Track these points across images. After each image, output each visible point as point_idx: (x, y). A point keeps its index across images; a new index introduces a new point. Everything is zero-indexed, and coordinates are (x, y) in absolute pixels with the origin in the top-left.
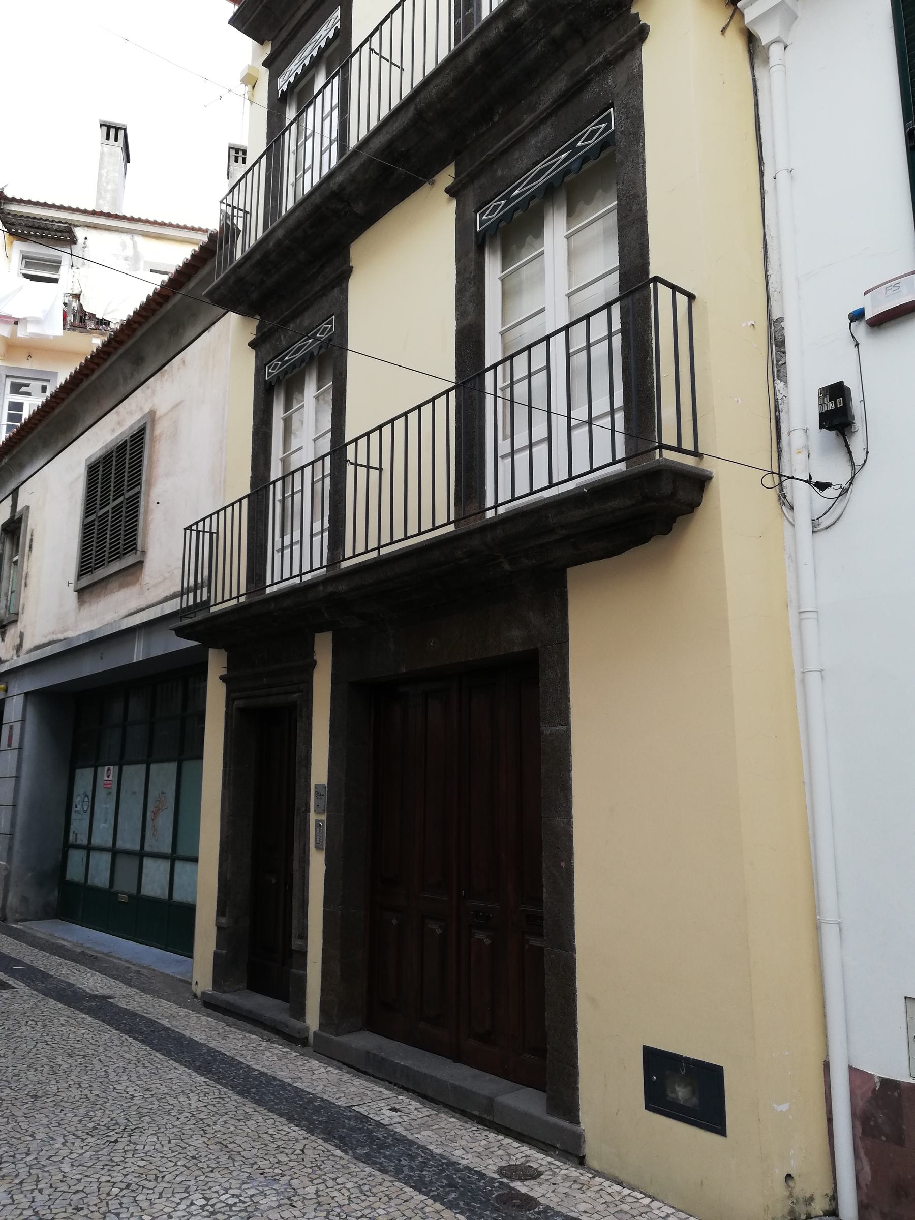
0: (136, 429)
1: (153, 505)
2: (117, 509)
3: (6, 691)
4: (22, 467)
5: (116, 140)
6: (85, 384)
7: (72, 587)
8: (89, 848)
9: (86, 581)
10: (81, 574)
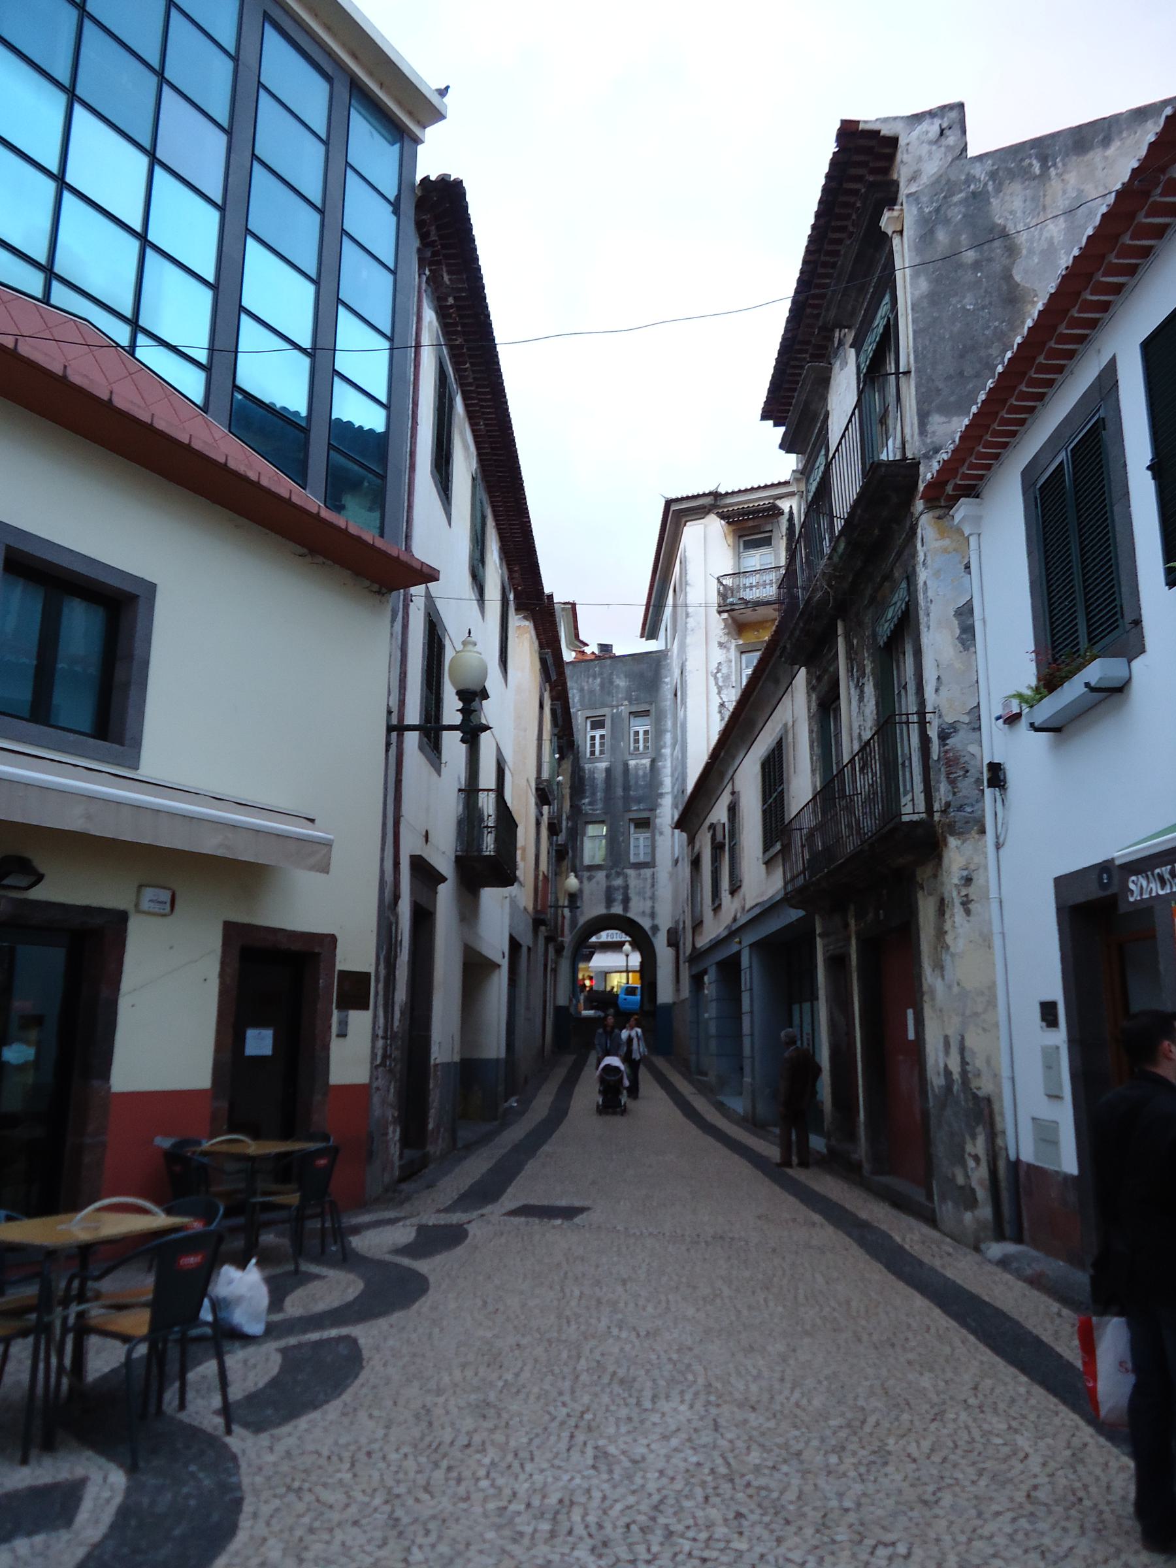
0: (779, 736)
3: (740, 942)
4: (734, 758)
7: (761, 861)
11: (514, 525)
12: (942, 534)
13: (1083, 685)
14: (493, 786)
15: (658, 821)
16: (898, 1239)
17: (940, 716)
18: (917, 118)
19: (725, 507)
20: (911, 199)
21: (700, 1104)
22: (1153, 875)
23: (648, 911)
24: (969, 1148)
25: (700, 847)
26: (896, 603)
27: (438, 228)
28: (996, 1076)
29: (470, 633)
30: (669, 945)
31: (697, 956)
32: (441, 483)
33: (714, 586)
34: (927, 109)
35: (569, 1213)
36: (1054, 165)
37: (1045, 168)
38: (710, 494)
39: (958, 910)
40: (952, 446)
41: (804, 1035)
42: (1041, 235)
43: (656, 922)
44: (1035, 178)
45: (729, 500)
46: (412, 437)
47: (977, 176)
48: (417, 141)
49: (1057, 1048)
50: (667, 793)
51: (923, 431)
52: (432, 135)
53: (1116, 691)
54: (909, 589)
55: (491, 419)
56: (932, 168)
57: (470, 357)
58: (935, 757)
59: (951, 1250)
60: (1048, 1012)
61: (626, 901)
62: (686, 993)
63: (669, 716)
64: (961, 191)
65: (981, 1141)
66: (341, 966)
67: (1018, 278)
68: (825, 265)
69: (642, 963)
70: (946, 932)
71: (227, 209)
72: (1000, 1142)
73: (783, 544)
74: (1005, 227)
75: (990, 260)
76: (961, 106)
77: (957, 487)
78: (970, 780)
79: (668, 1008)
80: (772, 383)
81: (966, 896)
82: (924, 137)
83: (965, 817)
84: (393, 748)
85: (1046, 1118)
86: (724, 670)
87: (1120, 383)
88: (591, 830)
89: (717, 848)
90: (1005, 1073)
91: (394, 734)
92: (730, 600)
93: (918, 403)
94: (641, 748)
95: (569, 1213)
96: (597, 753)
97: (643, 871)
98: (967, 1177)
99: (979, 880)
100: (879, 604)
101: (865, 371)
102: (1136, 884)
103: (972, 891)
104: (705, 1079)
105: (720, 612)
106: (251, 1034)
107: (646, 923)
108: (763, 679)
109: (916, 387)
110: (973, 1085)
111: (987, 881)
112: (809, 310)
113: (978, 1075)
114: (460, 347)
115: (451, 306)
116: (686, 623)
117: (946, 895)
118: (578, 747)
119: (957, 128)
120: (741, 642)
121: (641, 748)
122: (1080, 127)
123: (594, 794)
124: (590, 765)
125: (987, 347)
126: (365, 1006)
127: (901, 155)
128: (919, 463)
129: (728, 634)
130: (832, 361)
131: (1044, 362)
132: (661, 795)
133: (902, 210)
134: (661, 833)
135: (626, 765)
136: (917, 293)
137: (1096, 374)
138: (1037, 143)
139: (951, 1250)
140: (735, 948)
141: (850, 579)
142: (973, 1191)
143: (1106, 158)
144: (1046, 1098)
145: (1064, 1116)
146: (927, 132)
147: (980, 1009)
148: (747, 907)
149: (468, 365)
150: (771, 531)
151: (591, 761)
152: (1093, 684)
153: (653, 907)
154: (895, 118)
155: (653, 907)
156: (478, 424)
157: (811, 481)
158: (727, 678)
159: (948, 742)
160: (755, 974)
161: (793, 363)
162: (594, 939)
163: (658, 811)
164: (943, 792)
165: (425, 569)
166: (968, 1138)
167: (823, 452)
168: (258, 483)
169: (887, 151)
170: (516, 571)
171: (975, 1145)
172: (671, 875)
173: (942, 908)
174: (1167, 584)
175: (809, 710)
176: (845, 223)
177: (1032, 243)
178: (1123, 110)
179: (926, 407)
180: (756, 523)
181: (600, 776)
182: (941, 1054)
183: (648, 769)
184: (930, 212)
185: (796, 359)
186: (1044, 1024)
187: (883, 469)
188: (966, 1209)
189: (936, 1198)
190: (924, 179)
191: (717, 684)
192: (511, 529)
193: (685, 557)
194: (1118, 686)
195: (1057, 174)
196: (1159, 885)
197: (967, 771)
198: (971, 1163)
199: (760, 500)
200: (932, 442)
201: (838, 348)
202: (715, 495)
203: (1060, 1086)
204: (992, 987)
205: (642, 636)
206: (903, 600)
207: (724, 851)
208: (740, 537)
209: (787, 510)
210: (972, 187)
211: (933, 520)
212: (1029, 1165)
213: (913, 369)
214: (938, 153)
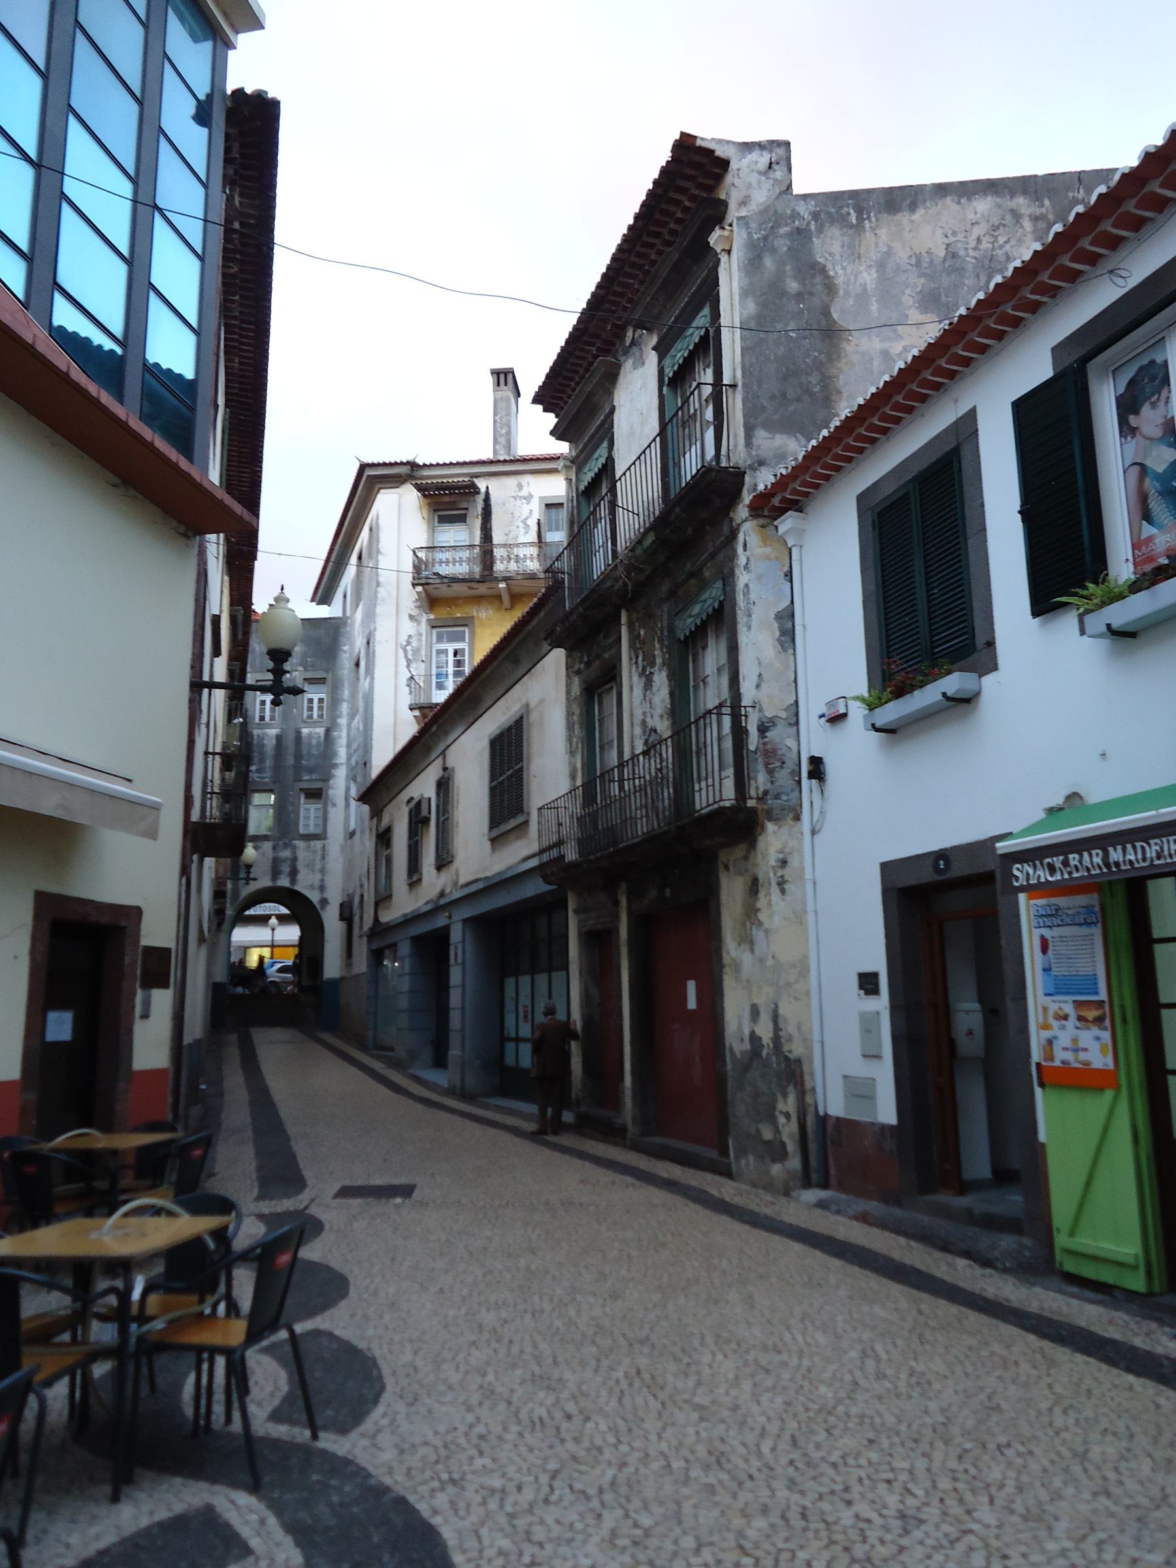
0: (518, 716)
1: (532, 778)
2: (510, 777)
3: (450, 917)
4: (447, 733)
5: (506, 385)
6: (483, 676)
7: (486, 837)
8: (518, 1040)
9: (496, 832)
10: (491, 828)
12: (765, 541)
13: (941, 695)
15: (331, 792)
16: (716, 1193)
17: (761, 710)
18: (747, 147)
19: (420, 479)
21: (396, 1077)
22: (1042, 864)
23: (317, 883)
24: (781, 1106)
26: (705, 601)
28: (807, 1042)
29: (282, 589)
30: (342, 917)
31: (378, 930)
34: (757, 139)
35: (406, 1191)
36: (869, 218)
37: (860, 219)
38: (408, 463)
39: (775, 889)
40: (793, 463)
42: (856, 280)
43: (326, 895)
44: (852, 226)
45: (426, 473)
47: (802, 214)
48: (229, 45)
49: (878, 1013)
51: (748, 443)
52: (244, 40)
53: (964, 702)
54: (724, 590)
55: (249, 358)
56: (761, 196)
58: (752, 747)
59: (771, 1199)
60: (868, 983)
61: (294, 873)
62: (361, 964)
63: (346, 685)
64: (787, 225)
65: (792, 1098)
66: (146, 941)
67: (835, 316)
68: (633, 265)
69: (301, 938)
70: (759, 910)
71: (50, 77)
72: (809, 1099)
73: (478, 522)
74: (825, 266)
75: (811, 294)
76: (787, 144)
77: (784, 500)
78: (785, 772)
79: (335, 983)
80: (552, 369)
81: (782, 877)
83: (781, 804)
85: (857, 1075)
86: (414, 644)
87: (980, 433)
88: (258, 799)
89: (418, 821)
90: (816, 1037)
92: (425, 574)
93: (744, 416)
94: (315, 716)
95: (406, 1191)
96: (267, 718)
97: (312, 843)
98: (777, 1130)
99: (794, 862)
100: (680, 599)
102: (1022, 872)
103: (787, 872)
104: (390, 1054)
105: (414, 585)
106: (52, 1016)
107: (314, 897)
109: (743, 401)
110: (786, 1048)
111: (801, 863)
112: (607, 305)
113: (790, 1039)
114: (233, 276)
116: (376, 592)
117: (761, 876)
118: (246, 711)
119: (783, 163)
120: (432, 616)
121: (315, 716)
122: (891, 188)
123: (262, 761)
125: (808, 374)
126: (166, 985)
127: (729, 178)
128: (745, 473)
129: (419, 607)
130: (622, 359)
131: (901, 401)
132: (335, 766)
133: (732, 231)
134: (334, 805)
135: (298, 734)
137: (953, 419)
138: (854, 194)
139: (771, 1199)
140: (440, 921)
141: (648, 572)
142: (783, 1144)
143: (912, 222)
144: (861, 1058)
145: (884, 1076)
146: (757, 162)
147: (792, 979)
148: (462, 881)
149: (237, 298)
150: (467, 509)
151: (260, 726)
152: (949, 694)
153: (322, 880)
154: (728, 142)
155: (322, 880)
156: (232, 361)
157: (586, 470)
158: (416, 651)
159: (767, 734)
160: (469, 947)
161: (578, 353)
162: (247, 913)
164: (760, 781)
166: (779, 1097)
169: (718, 171)
171: (786, 1103)
172: (343, 848)
173: (754, 887)
174: (1033, 615)
175: (568, 693)
176: (661, 230)
177: (848, 285)
178: (928, 182)
179: (751, 421)
180: (451, 499)
181: (270, 744)
183: (322, 738)
184: (759, 239)
185: (582, 350)
186: (862, 992)
187: (714, 474)
188: (774, 1161)
189: (731, 1153)
190: (753, 206)
191: (406, 656)
193: (377, 524)
194: (966, 697)
195: (871, 227)
196: (1047, 872)
197: (784, 763)
198: (782, 1120)
199: (457, 476)
200: (757, 455)
201: (630, 346)
202: (413, 465)
203: (880, 1047)
204: (805, 958)
205: (312, 601)
206: (714, 599)
207: (428, 826)
208: (435, 511)
209: (483, 490)
210: (797, 223)
211: (757, 528)
212: (838, 1119)
213: (740, 384)
214: (767, 185)
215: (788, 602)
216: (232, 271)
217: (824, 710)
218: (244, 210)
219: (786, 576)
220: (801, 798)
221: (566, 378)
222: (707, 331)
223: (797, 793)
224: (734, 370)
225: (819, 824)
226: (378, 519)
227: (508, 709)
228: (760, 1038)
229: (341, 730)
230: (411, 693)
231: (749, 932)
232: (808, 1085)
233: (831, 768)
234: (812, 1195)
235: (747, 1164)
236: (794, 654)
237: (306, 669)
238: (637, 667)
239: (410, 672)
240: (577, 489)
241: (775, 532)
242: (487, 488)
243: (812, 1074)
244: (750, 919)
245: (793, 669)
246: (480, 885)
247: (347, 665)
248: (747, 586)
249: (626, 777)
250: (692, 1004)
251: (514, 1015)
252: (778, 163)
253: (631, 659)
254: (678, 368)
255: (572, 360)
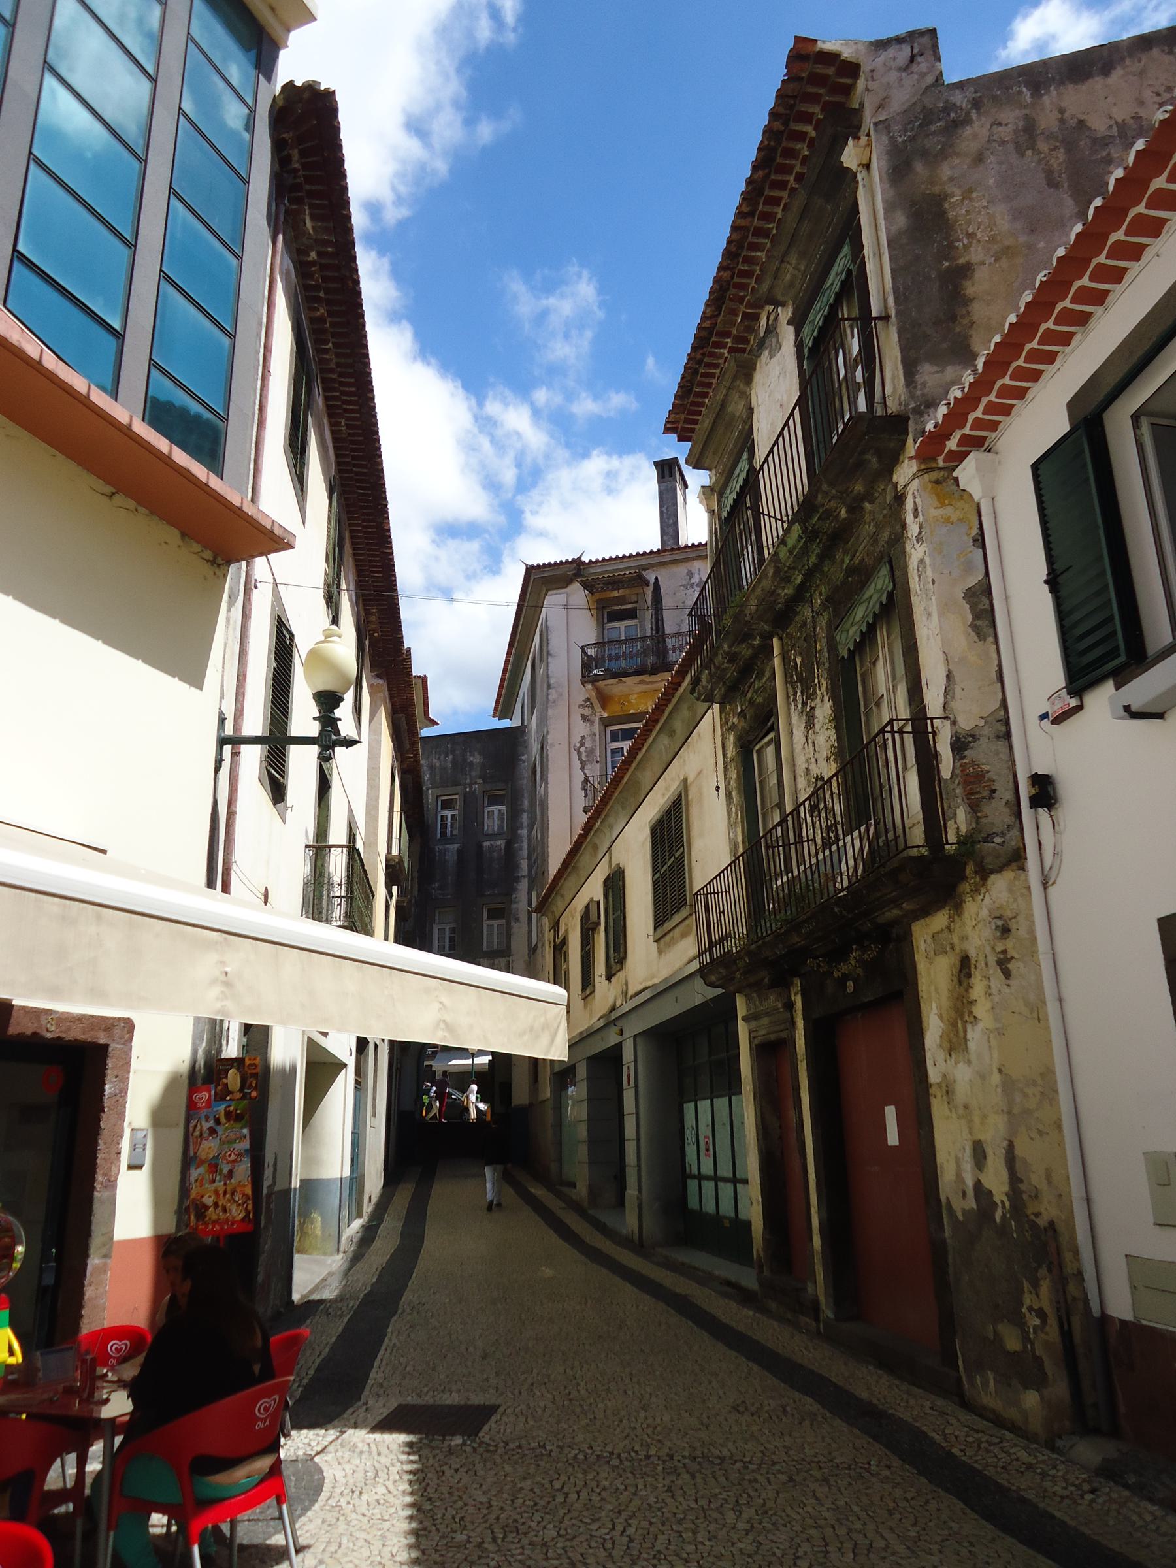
8: (700, 1177)
9: (660, 932)
10: (655, 928)
11: (375, 561)
14: (344, 841)
17: (954, 723)
18: (881, 45)
20: (880, 127)
24: (1028, 1300)
25: (567, 930)
26: (871, 597)
27: (303, 154)
28: (1063, 1198)
32: (295, 467)
33: (577, 655)
34: (892, 35)
39: (996, 973)
41: (701, 1139)
46: (262, 389)
47: (958, 104)
50: (524, 877)
52: (297, 38)
56: (902, 96)
57: (334, 335)
63: (526, 795)
64: (940, 119)
65: (1045, 1287)
68: (759, 232)
76: (933, 32)
81: (1004, 952)
82: (893, 64)
84: (226, 765)
86: (588, 744)
90: (1077, 1192)
91: (228, 748)
99: (1020, 929)
101: (810, 344)
105: (583, 683)
108: (654, 733)
112: (733, 291)
113: (1036, 1196)
114: (321, 320)
115: (313, 263)
116: (548, 694)
124: (441, 847)
132: (517, 879)
134: (517, 920)
135: (481, 847)
136: (894, 229)
140: (612, 1039)
142: (1038, 1361)
148: (631, 992)
156: (338, 424)
158: (590, 752)
159: (966, 753)
161: (707, 360)
163: (514, 896)
164: (959, 822)
165: (277, 531)
167: (745, 456)
168: (39, 363)
169: (848, 81)
170: (372, 614)
182: (968, 1166)
185: (712, 355)
191: (580, 759)
192: (371, 561)
193: (547, 626)
197: (994, 791)
200: (923, 395)
202: (577, 562)
204: (1048, 1073)
209: (652, 581)
210: (952, 115)
211: (930, 486)
212: (1123, 1323)
213: (893, 312)
215: (980, 575)
216: (319, 313)
217: (1045, 707)
218: (319, 237)
219: (975, 540)
220: (1023, 839)
221: (698, 395)
222: (849, 271)
223: (1015, 832)
224: (885, 300)
225: (1055, 869)
226: (547, 621)
227: (667, 789)
228: (990, 1193)
229: (522, 842)
230: (586, 796)
231: (961, 1034)
232: (1070, 1268)
233: (1069, 788)
234: (1089, 1452)
235: (985, 1384)
236: (997, 643)
237: (485, 782)
238: (796, 705)
239: (585, 774)
240: (720, 519)
241: (954, 488)
242: (656, 578)
243: (1076, 1252)
244: (962, 1016)
245: (996, 662)
246: (647, 995)
247: (526, 775)
248: (921, 561)
249: (792, 841)
250: (893, 1139)
251: (695, 1147)
252: (921, 55)
253: (788, 697)
254: (819, 332)
255: (702, 370)
